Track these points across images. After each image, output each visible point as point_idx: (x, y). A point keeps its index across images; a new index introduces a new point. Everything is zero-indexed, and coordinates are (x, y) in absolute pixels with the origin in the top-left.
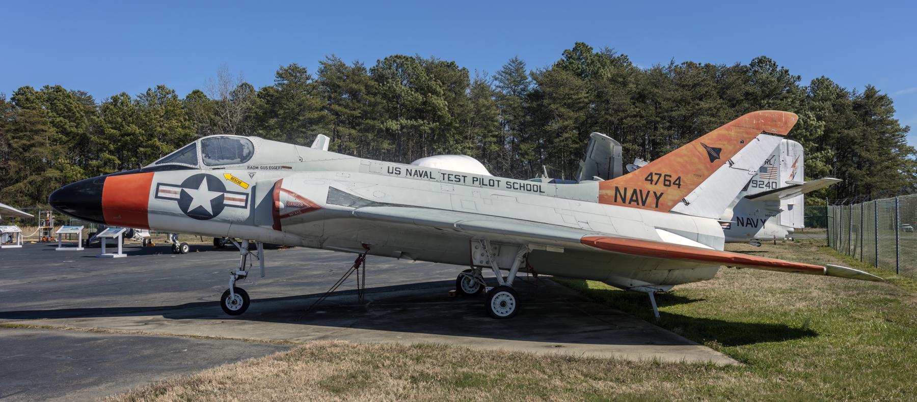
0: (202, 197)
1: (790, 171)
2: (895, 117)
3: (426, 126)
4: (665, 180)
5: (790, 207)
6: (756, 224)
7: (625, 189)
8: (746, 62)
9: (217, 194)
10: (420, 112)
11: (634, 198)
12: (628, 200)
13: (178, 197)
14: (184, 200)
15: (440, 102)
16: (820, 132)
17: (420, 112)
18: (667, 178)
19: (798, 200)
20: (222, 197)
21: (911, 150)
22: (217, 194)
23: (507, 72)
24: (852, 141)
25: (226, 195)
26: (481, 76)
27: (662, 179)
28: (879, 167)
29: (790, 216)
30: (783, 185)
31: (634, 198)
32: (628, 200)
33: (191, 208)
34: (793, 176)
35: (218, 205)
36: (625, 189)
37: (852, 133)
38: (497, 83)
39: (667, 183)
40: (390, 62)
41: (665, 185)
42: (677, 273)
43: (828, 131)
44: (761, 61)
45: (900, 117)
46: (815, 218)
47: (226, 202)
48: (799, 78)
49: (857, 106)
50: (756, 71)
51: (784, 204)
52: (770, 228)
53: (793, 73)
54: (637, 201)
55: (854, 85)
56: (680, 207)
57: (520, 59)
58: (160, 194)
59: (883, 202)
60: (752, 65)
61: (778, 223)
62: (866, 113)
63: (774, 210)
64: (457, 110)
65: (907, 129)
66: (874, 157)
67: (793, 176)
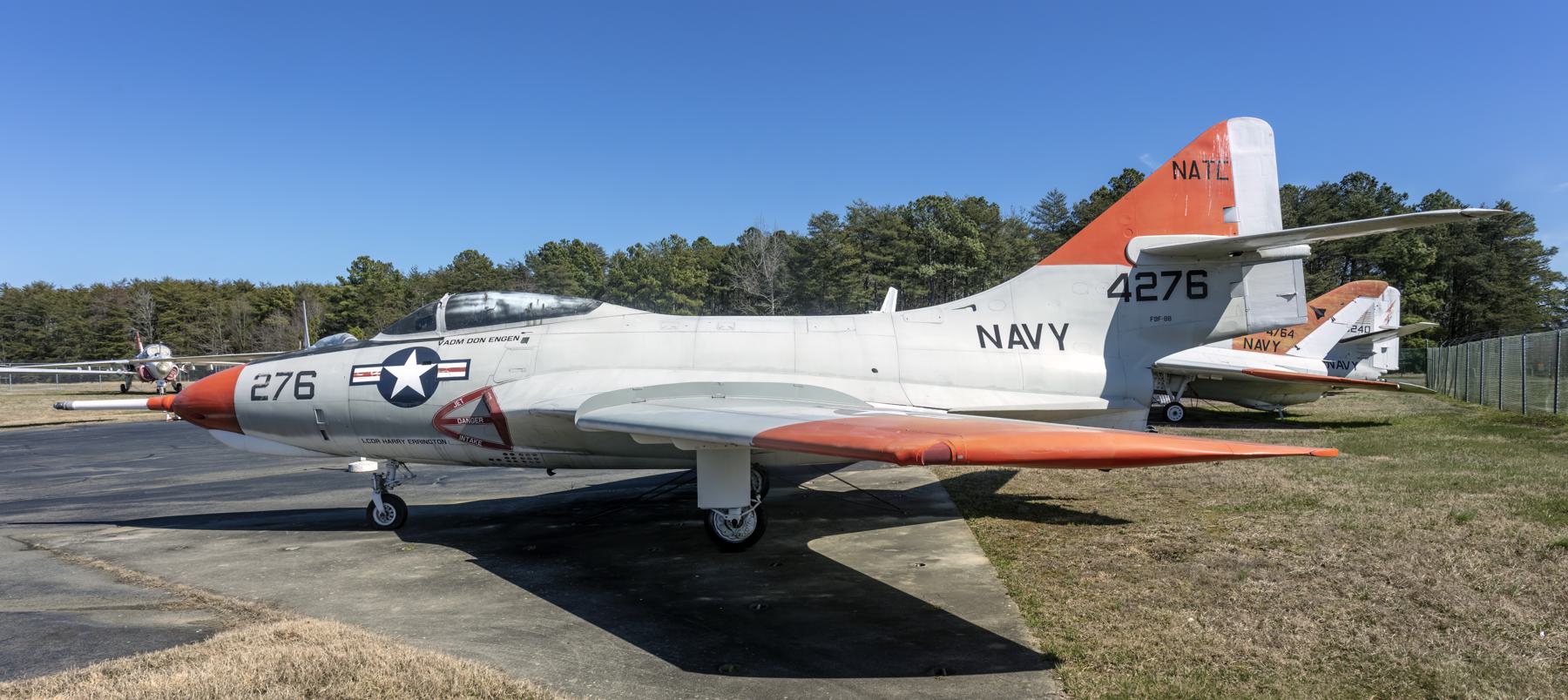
0: (409, 375)
1: (1385, 315)
2: (1536, 237)
3: (962, 270)
4: (1190, 285)
5: (1384, 350)
6: (1347, 366)
7: (996, 327)
8: (1336, 179)
9: (428, 368)
10: (950, 256)
11: (1016, 338)
12: (1005, 340)
13: (378, 379)
14: (387, 382)
15: (976, 245)
16: (1431, 261)
17: (950, 256)
18: (1195, 279)
19: (1393, 344)
20: (435, 370)
21: (1558, 277)
22: (428, 368)
23: (1045, 206)
24: (1471, 270)
25: (440, 366)
26: (1018, 213)
27: (1183, 281)
28: (1509, 299)
29: (1386, 357)
30: (1376, 329)
31: (1016, 338)
32: (1005, 340)
33: (396, 392)
34: (1388, 320)
35: (430, 381)
36: (996, 327)
37: (1470, 260)
38: (1034, 219)
39: (1198, 291)
40: (921, 204)
41: (1190, 296)
42: (1290, 397)
43: (1440, 259)
44: (1355, 178)
45: (1544, 237)
46: (1412, 361)
47: (440, 375)
48: (1405, 196)
49: (1483, 227)
50: (1347, 192)
51: (1377, 347)
52: (1362, 370)
53: (1397, 190)
54: (1022, 342)
55: (1477, 202)
56: (1293, 351)
57: (1060, 191)
58: (464, 365)
59: (1511, 345)
60: (1344, 182)
61: (1371, 365)
62: (1495, 236)
63: (1367, 353)
64: (994, 253)
65: (1553, 251)
66: (1500, 288)
67: (1388, 320)
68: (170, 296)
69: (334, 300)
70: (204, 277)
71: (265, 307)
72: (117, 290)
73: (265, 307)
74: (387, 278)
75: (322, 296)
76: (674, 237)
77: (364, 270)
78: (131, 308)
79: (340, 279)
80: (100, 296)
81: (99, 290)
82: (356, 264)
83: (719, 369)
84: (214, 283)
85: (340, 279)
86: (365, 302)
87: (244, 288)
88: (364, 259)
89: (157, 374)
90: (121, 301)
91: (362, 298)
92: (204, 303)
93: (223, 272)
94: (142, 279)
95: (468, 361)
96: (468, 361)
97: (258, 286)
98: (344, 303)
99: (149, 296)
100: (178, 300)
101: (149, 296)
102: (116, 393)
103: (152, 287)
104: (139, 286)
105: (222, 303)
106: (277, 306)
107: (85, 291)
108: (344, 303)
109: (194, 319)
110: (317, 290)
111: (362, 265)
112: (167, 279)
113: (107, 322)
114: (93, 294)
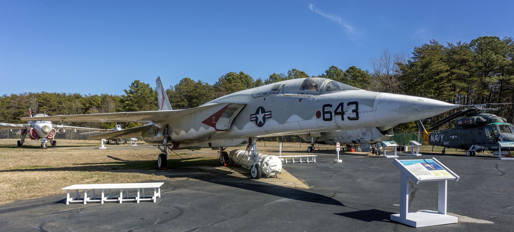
25: (266, 114)
47: (266, 117)
68: (45, 99)
69: (122, 101)
70: (60, 92)
71: (87, 105)
72: (22, 97)
73: (87, 105)
74: (147, 91)
75: (115, 100)
76: (294, 70)
77: (137, 87)
78: (28, 105)
79: (126, 91)
80: (14, 99)
81: (14, 97)
82: (133, 84)
83: (236, 146)
84: (64, 94)
85: (126, 91)
86: (137, 102)
87: (78, 97)
88: (137, 82)
89: (41, 134)
90: (23, 101)
91: (136, 100)
92: (60, 103)
93: (69, 90)
94: (33, 92)
95: (271, 112)
96: (271, 112)
97: (83, 96)
98: (127, 102)
99: (36, 99)
100: (49, 101)
101: (36, 99)
102: (13, 147)
103: (38, 96)
104: (31, 95)
105: (69, 103)
106: (93, 105)
107: (8, 97)
108: (127, 102)
109: (55, 110)
110: (114, 99)
111: (136, 84)
112: (43, 92)
113: (17, 111)
114: (11, 98)
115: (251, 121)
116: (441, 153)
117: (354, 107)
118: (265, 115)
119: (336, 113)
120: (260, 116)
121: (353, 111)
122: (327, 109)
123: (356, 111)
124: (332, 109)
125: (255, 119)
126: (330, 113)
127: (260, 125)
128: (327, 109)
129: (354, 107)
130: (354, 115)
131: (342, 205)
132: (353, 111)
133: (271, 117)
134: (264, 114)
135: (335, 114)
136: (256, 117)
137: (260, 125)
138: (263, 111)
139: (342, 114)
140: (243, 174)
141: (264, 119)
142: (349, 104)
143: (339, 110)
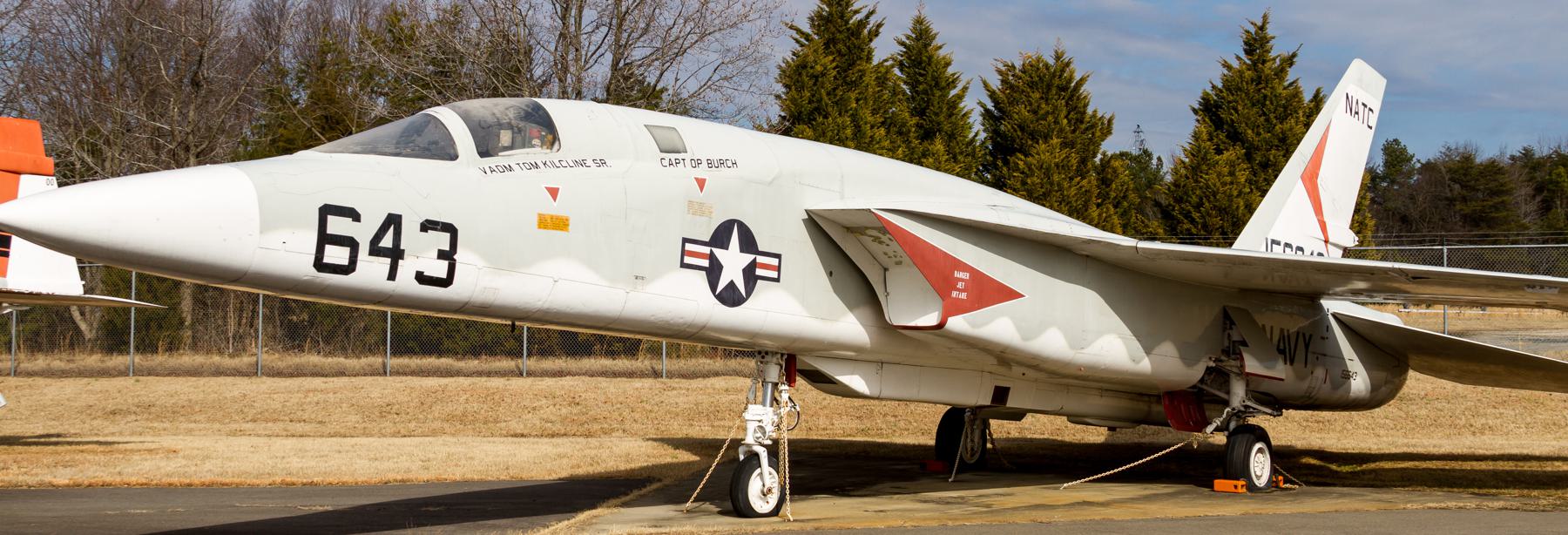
25: (760, 259)
47: (759, 272)
115: (684, 265)
116: (1416, 382)
117: (443, 241)
118: (753, 265)
119: (375, 251)
120: (733, 261)
121: (442, 255)
122: (336, 225)
123: (447, 255)
124: (363, 233)
125: (705, 263)
126: (351, 243)
127: (731, 297)
128: (336, 225)
129: (443, 241)
130: (439, 269)
131: (662, 440)
132: (442, 255)
133: (777, 280)
134: (749, 258)
135: (372, 253)
136: (712, 257)
137: (731, 297)
138: (748, 244)
139: (396, 254)
140: (1075, 418)
141: (750, 274)
142: (427, 226)
143: (387, 242)
